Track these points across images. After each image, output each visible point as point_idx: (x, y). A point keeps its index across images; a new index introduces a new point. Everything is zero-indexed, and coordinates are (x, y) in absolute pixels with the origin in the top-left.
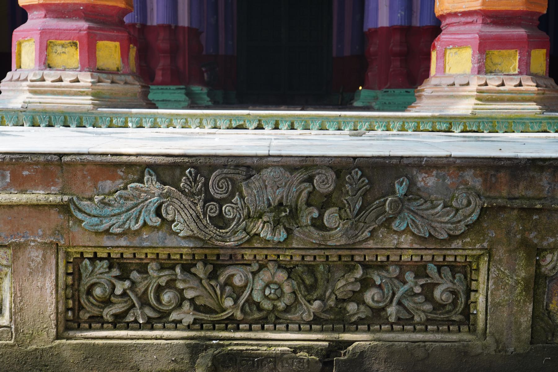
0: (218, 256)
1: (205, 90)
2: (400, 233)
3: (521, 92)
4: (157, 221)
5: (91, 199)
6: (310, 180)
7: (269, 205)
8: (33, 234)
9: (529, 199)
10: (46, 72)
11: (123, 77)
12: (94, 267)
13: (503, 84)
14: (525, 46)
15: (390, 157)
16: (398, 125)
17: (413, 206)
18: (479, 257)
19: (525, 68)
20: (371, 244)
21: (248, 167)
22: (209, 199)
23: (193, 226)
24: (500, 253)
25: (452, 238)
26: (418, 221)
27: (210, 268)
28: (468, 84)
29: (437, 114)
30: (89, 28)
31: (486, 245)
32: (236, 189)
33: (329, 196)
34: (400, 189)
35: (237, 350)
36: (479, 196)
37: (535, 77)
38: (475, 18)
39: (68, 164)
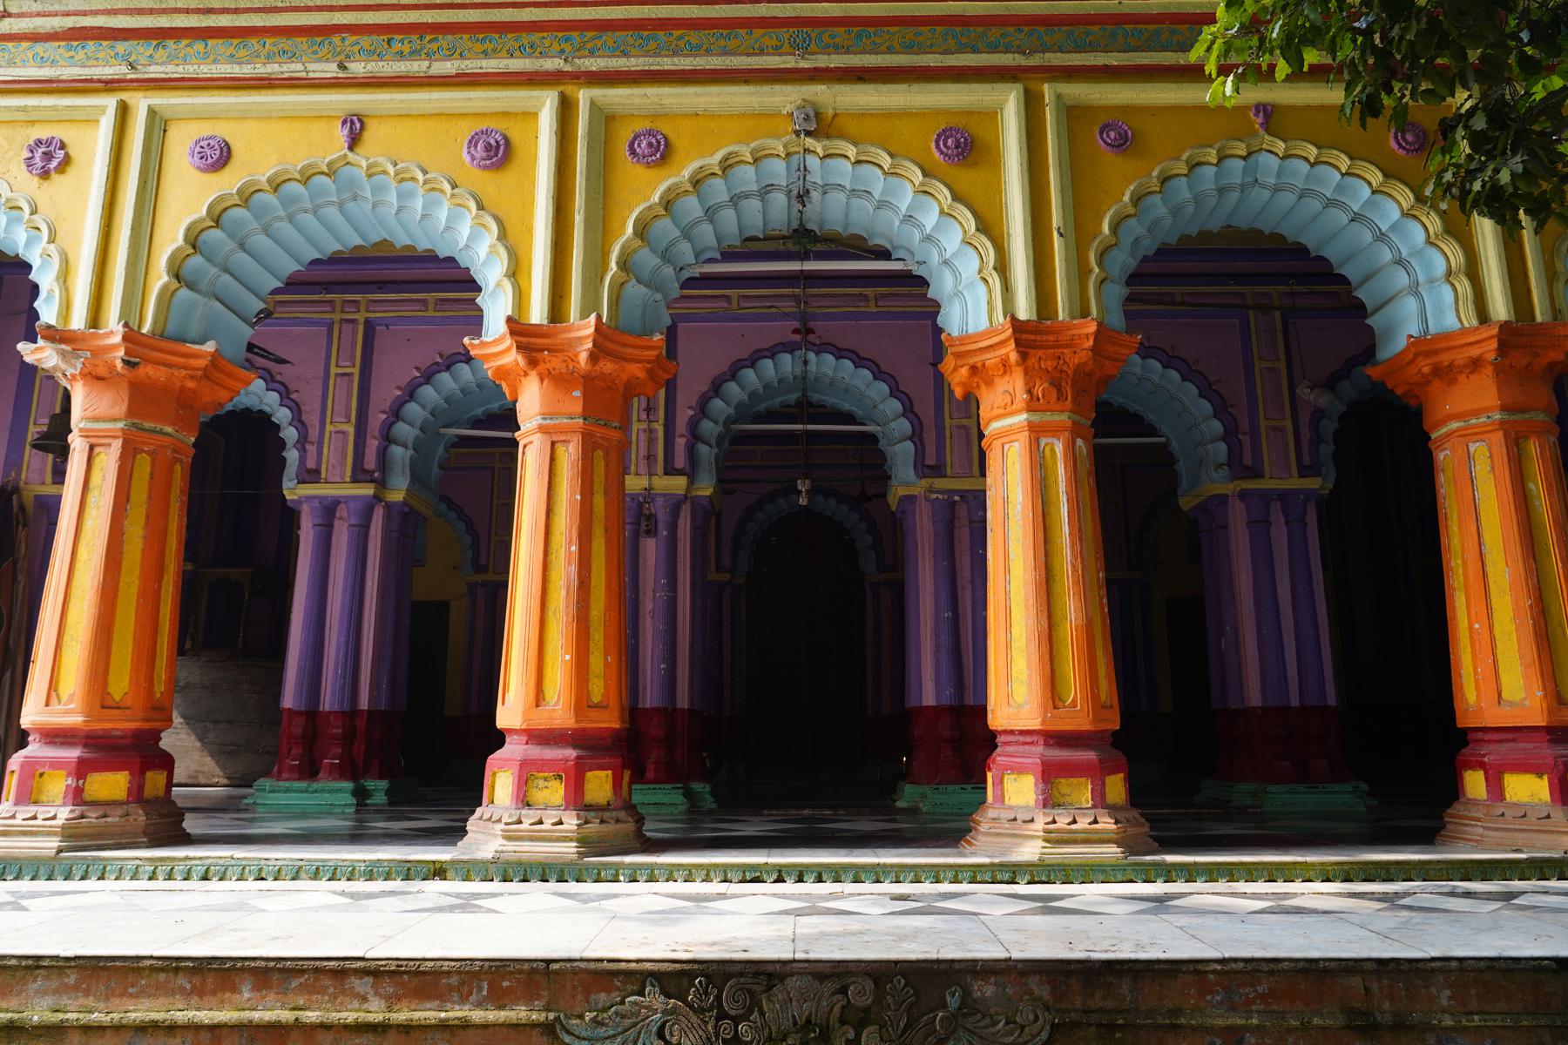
1: (708, 788)
3: (1097, 831)
6: (843, 991)
7: (795, 1023)
9: (1108, 1011)
10: (524, 812)
11: (614, 814)
13: (1074, 822)
14: (1097, 774)
15: (938, 961)
16: (950, 875)
17: (969, 1023)
19: (1100, 801)
21: (770, 975)
22: (723, 1015)
28: (1032, 821)
29: (996, 861)
30: (578, 757)
32: (755, 1004)
33: (867, 1010)
34: (953, 1002)
36: (1048, 1008)
37: (1113, 809)
38: (1035, 738)
39: (556, 972)
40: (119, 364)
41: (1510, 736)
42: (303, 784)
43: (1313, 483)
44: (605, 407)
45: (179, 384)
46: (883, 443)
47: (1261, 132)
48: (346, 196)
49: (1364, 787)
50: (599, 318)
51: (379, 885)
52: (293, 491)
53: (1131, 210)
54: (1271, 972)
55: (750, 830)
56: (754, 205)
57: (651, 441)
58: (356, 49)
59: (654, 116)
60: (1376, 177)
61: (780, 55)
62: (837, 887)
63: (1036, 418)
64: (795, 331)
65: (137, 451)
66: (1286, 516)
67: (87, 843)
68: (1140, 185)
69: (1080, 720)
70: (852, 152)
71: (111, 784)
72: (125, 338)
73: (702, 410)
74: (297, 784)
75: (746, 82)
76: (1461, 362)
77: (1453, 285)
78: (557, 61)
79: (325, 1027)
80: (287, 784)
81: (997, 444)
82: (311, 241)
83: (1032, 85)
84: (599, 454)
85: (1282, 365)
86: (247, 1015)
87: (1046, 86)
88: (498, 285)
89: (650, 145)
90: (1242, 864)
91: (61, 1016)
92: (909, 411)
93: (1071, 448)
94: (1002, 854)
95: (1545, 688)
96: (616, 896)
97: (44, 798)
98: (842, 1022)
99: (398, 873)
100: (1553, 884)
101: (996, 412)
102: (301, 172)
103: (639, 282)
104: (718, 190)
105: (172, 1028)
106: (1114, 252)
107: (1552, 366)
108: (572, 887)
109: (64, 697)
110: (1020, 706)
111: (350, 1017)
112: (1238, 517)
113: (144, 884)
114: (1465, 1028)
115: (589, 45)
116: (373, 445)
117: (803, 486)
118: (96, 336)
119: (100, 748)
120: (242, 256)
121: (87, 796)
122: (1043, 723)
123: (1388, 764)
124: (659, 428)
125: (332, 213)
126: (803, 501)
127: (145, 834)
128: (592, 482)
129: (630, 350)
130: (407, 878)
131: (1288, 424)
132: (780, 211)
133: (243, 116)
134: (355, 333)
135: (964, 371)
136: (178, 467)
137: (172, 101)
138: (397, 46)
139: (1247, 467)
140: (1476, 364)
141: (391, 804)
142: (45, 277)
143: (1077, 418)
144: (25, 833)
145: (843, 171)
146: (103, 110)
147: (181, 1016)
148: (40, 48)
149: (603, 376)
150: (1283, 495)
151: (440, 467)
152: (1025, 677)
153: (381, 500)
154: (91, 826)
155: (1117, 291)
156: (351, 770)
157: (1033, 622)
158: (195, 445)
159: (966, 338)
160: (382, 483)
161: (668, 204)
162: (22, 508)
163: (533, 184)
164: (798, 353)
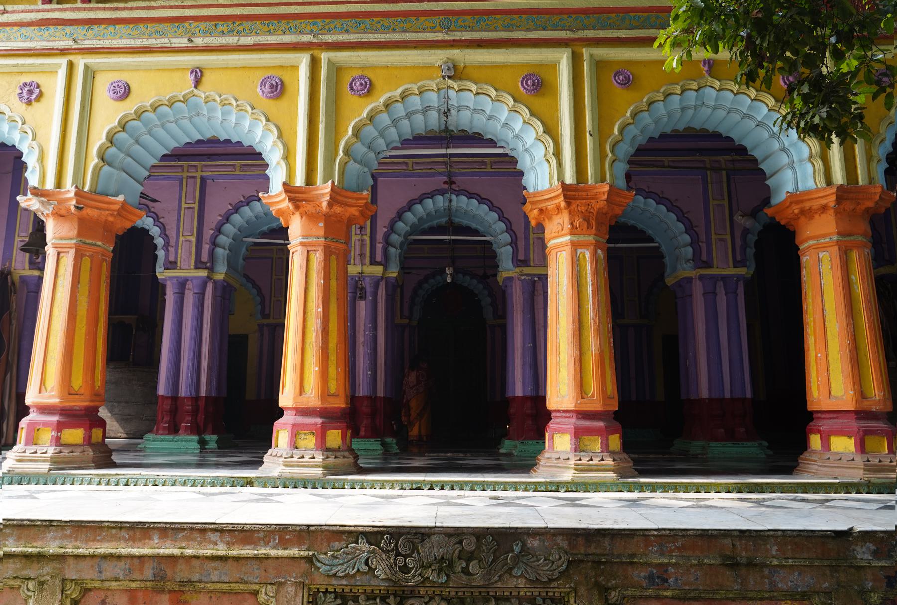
0: (403, 591)
1: (395, 441)
2: (518, 577)
3: (603, 465)
4: (366, 568)
5: (326, 554)
6: (461, 542)
7: (436, 559)
8: (290, 576)
9: (597, 555)
10: (294, 451)
12: (326, 597)
13: (591, 460)
15: (510, 528)
16: (523, 487)
17: (525, 559)
18: (569, 593)
19: (606, 448)
20: (499, 584)
21: (422, 534)
22: (398, 554)
23: (388, 572)
24: (582, 590)
25: (551, 580)
26: (529, 570)
27: (398, 599)
29: (548, 480)
30: (323, 423)
31: (572, 585)
32: (414, 549)
33: (472, 553)
34: (517, 549)
35: (447, 452)
37: (612, 453)
38: (571, 415)
39: (313, 532)
40: (73, 209)
41: (835, 416)
42: (171, 437)
43: (742, 271)
44: (336, 232)
45: (104, 218)
46: (495, 247)
47: (706, 75)
48: (194, 113)
49: (766, 444)
50: (333, 183)
51: (218, 489)
52: (162, 273)
53: (631, 121)
54: (683, 536)
55: (416, 463)
56: (420, 117)
57: (363, 246)
58: (198, 30)
59: (363, 68)
60: (771, 101)
61: (435, 32)
62: (462, 493)
63: (575, 238)
64: (445, 183)
65: (82, 256)
66: (725, 289)
67: (64, 465)
68: (636, 107)
69: (595, 404)
70: (474, 88)
71: (75, 435)
72: (76, 194)
73: (392, 228)
74: (167, 437)
75: (415, 48)
76: (815, 207)
77: (813, 163)
78: (309, 36)
79: (196, 557)
80: (162, 437)
81: (554, 252)
82: (173, 137)
83: (577, 49)
84: (334, 257)
85: (726, 202)
86: (156, 551)
87: (584, 50)
88: (278, 163)
89: (361, 84)
90: (682, 483)
91: (64, 550)
92: (510, 229)
93: (594, 255)
94: (552, 477)
95: (854, 390)
96: (343, 496)
97: (40, 442)
98: (460, 558)
99: (228, 483)
100: (853, 496)
101: (554, 234)
102: (169, 100)
103: (355, 161)
104: (399, 109)
105: (119, 557)
106: (621, 144)
107: (867, 210)
108: (320, 491)
109: (49, 389)
110: (563, 397)
111: (209, 552)
112: (698, 290)
113: (95, 487)
114: (784, 566)
115: (327, 27)
116: (206, 248)
117: (449, 271)
118: (60, 193)
119: (69, 416)
120: (137, 147)
121: (62, 441)
122: (575, 406)
123: (770, 428)
124: (367, 238)
125: (185, 123)
126: (449, 280)
127: (93, 462)
128: (330, 273)
129: (350, 200)
130: (233, 486)
131: (728, 237)
132: (434, 120)
133: (136, 69)
134: (195, 184)
135: (536, 212)
136: (104, 264)
137: (98, 60)
138: (220, 28)
139: (704, 262)
140: (824, 208)
141: (219, 448)
142: (31, 159)
143: (598, 238)
144: (31, 460)
145: (469, 98)
146: (60, 66)
147: (124, 551)
148: (23, 30)
149: (336, 215)
150: (724, 278)
151: (244, 260)
152: (566, 382)
153: (211, 279)
154: (65, 457)
155: (622, 167)
156: (196, 429)
157: (571, 351)
158: (112, 251)
159: (537, 193)
160: (211, 270)
161: (371, 118)
162: (13, 283)
163: (296, 107)
164: (446, 195)
